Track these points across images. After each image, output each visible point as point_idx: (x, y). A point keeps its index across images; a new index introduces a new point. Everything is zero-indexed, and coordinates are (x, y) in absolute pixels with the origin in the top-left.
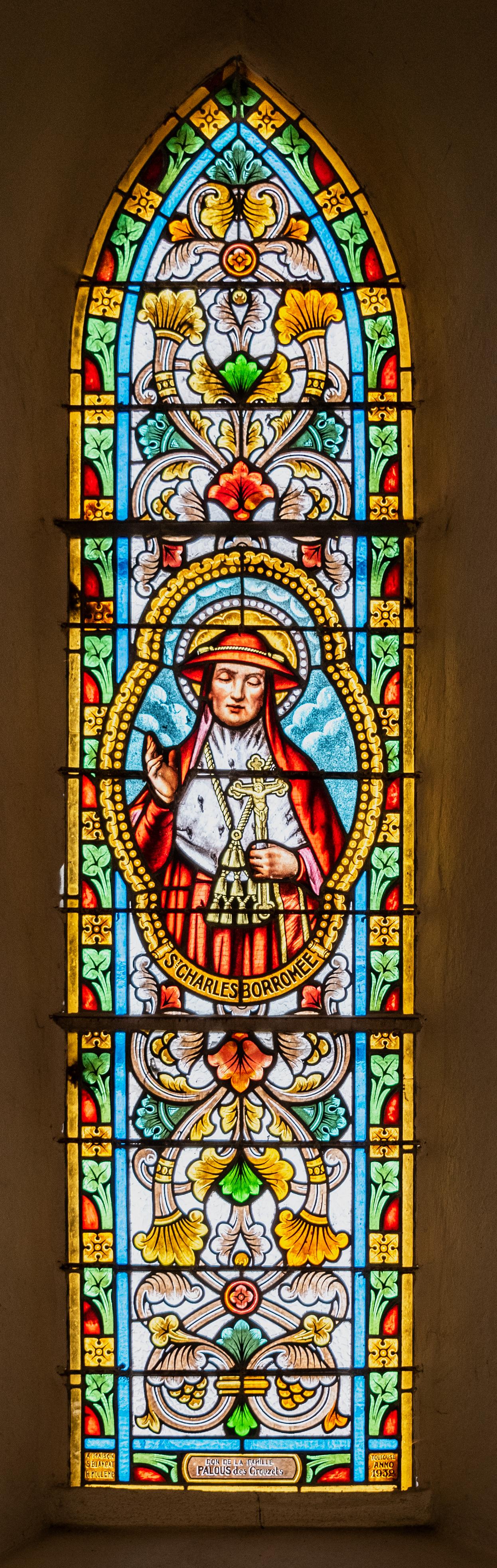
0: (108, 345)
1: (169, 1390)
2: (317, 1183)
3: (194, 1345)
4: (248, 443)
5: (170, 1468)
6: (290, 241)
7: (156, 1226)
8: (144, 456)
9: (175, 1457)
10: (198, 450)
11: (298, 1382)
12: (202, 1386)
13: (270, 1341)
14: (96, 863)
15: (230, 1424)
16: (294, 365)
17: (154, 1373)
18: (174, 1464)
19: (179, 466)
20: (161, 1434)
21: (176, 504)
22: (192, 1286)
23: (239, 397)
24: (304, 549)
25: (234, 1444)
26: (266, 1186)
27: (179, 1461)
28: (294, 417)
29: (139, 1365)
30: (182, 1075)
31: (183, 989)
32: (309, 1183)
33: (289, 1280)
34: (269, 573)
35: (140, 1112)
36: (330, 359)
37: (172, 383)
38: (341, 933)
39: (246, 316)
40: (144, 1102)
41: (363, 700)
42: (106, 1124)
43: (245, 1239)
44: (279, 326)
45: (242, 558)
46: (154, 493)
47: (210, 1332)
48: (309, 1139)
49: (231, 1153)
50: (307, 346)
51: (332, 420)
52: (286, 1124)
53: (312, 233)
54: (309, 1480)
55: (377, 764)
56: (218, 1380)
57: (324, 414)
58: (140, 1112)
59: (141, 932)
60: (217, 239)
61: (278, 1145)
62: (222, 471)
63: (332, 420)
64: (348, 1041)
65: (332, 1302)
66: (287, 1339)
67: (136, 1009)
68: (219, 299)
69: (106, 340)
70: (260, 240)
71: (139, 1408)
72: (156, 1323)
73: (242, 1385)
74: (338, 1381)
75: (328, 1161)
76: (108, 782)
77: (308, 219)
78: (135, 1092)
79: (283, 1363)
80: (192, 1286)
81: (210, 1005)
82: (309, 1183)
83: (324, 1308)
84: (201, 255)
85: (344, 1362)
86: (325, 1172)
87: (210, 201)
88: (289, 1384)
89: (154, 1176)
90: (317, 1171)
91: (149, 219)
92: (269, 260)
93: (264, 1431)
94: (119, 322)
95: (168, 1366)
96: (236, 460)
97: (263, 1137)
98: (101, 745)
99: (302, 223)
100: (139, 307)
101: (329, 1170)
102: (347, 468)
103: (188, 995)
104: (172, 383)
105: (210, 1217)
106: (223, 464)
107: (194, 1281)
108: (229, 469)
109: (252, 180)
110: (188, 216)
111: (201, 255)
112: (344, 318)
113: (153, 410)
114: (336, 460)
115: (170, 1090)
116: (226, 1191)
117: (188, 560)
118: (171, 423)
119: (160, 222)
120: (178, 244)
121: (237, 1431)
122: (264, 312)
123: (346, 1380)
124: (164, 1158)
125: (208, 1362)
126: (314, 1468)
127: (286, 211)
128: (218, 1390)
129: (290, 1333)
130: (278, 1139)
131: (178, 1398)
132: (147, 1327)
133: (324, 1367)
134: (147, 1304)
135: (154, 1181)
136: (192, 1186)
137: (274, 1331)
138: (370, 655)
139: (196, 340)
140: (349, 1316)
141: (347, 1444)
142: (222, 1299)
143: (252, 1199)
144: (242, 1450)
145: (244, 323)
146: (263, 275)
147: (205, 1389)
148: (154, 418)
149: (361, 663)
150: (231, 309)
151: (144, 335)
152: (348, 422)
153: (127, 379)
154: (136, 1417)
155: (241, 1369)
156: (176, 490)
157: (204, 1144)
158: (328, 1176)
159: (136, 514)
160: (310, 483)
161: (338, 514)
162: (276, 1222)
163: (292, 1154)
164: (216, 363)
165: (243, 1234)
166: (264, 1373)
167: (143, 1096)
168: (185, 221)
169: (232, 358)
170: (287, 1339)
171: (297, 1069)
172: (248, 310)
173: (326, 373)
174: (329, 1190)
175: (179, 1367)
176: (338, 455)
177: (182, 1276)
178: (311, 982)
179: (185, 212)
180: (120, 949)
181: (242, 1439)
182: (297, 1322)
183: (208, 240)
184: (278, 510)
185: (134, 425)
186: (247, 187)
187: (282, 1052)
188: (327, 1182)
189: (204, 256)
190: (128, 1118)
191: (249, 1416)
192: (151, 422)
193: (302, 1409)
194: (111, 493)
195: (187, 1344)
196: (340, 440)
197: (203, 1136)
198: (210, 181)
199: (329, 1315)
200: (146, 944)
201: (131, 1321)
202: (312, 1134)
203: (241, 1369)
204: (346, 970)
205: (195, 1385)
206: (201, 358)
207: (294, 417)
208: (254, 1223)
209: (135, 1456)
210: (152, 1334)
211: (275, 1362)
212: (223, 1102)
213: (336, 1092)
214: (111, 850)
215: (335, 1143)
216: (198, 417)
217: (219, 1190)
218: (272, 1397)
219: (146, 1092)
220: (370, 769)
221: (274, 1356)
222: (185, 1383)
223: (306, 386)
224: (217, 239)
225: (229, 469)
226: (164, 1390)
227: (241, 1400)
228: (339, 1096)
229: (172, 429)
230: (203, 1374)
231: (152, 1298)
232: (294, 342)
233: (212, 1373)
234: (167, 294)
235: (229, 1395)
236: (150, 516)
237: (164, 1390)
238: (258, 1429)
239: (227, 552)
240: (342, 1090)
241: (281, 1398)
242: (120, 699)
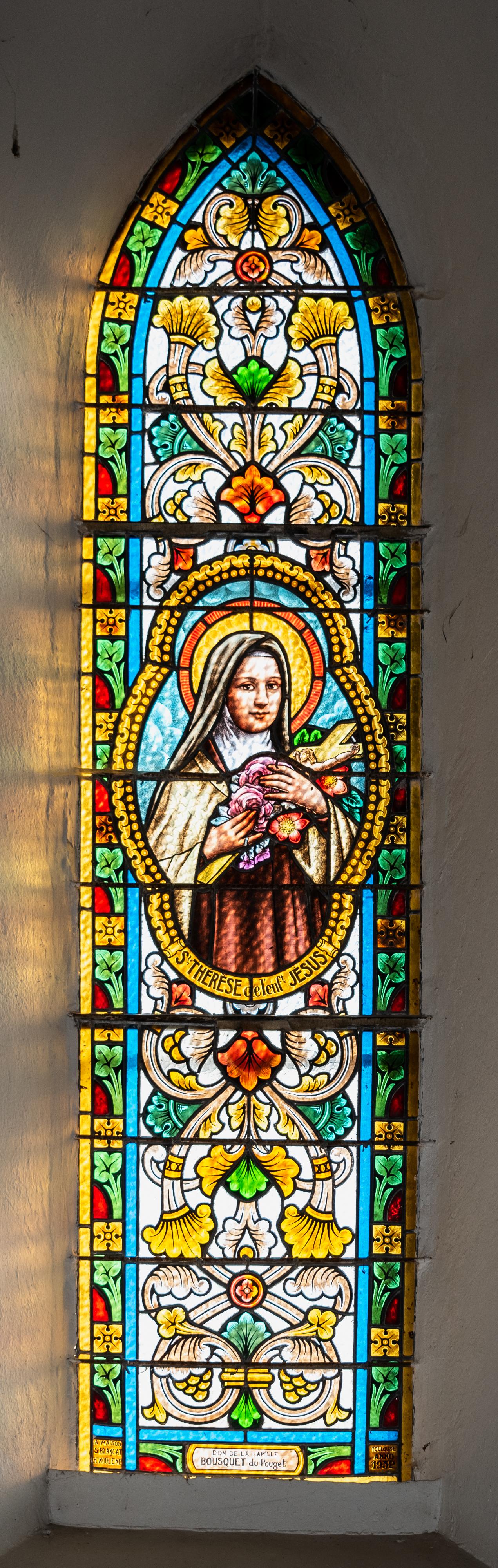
0: (123, 348)
1: (175, 1382)
2: (323, 1180)
3: (201, 1337)
4: (260, 447)
5: (175, 1458)
6: (303, 250)
7: (164, 1221)
8: (157, 457)
9: (180, 1448)
10: (208, 452)
11: (301, 1375)
12: (207, 1377)
13: (273, 1335)
14: (109, 866)
15: (234, 1416)
16: (306, 370)
17: (162, 1364)
18: (179, 1455)
19: (191, 469)
20: (166, 1425)
21: (190, 507)
22: (199, 1279)
23: (252, 401)
24: (313, 553)
25: (238, 1436)
26: (272, 1182)
27: (184, 1452)
28: (305, 421)
29: (145, 1355)
30: (192, 1073)
31: (193, 988)
32: (314, 1180)
33: (293, 1275)
34: (278, 576)
35: (151, 1108)
36: (341, 365)
37: (185, 387)
38: (349, 930)
39: (260, 321)
40: (154, 1099)
41: (370, 703)
42: (117, 1117)
43: (251, 1235)
44: (292, 331)
45: (252, 561)
46: (167, 494)
47: (215, 1325)
48: (315, 1138)
49: (238, 1151)
50: (319, 352)
51: (342, 426)
52: (294, 1123)
53: (325, 244)
54: (310, 1471)
55: (384, 765)
56: (223, 1372)
57: (334, 420)
58: (151, 1108)
59: (153, 931)
60: (232, 248)
61: (285, 1143)
62: (234, 474)
63: (342, 426)
64: (355, 1043)
65: (335, 1297)
66: (292, 1333)
67: (147, 1008)
68: (233, 306)
69: (121, 343)
70: (275, 248)
71: (145, 1399)
72: (163, 1315)
73: (246, 1377)
74: (339, 1374)
75: (333, 1157)
76: (120, 783)
77: (321, 229)
78: (146, 1089)
79: (288, 1356)
80: (199, 1279)
81: (220, 1003)
82: (314, 1180)
83: (328, 1303)
84: (214, 262)
85: (347, 1357)
86: (331, 1169)
87: (226, 211)
88: (291, 1377)
89: (163, 1172)
90: (323, 1168)
91: (165, 226)
92: (280, 267)
93: (268, 1424)
94: (133, 325)
95: (174, 1357)
96: (247, 465)
97: (272, 1135)
98: (113, 747)
99: (315, 232)
100: (154, 311)
101: (334, 1166)
102: (357, 474)
103: (198, 994)
104: (185, 387)
105: (217, 1214)
106: (235, 468)
107: (201, 1274)
108: (241, 472)
109: (267, 189)
110: (203, 225)
111: (214, 262)
112: (356, 326)
113: (164, 411)
114: (346, 466)
115: (181, 1088)
116: (234, 1187)
117: (199, 563)
118: (184, 424)
119: (176, 230)
120: (192, 252)
121: (241, 1422)
122: (278, 318)
123: (348, 1374)
124: (173, 1155)
125: (212, 1354)
126: (315, 1460)
127: (299, 222)
128: (223, 1382)
129: (293, 1327)
130: (284, 1138)
131: (184, 1390)
132: (155, 1319)
133: (327, 1361)
134: (155, 1296)
135: (164, 1177)
136: (200, 1183)
137: (277, 1325)
138: (377, 662)
139: (211, 345)
140: (352, 1310)
141: (348, 1437)
142: (228, 1293)
143: (259, 1194)
144: (245, 1442)
145: (258, 328)
146: (275, 280)
147: (210, 1380)
148: (167, 419)
149: (368, 668)
150: (245, 315)
151: (158, 340)
152: (358, 428)
153: (140, 379)
154: (143, 1408)
155: (247, 1361)
156: (188, 492)
157: (212, 1142)
158: (333, 1173)
159: (149, 514)
160: (319, 488)
161: (348, 519)
162: (282, 1217)
163: (297, 1152)
164: (230, 368)
165: (249, 1230)
166: (269, 1365)
167: (154, 1094)
168: (200, 230)
169: (245, 363)
170: (292, 1333)
171: (304, 1070)
172: (262, 316)
173: (337, 380)
174: (334, 1186)
175: (185, 1359)
176: (348, 460)
177: (189, 1269)
178: (319, 980)
179: (201, 221)
180: (132, 948)
181: (245, 1430)
182: (301, 1317)
183: (223, 249)
184: (287, 516)
185: (147, 426)
186: (262, 197)
187: (290, 1054)
188: (332, 1177)
189: (218, 263)
190: (139, 1115)
191: (251, 1406)
192: (164, 423)
193: (305, 1401)
194: (125, 492)
195: (193, 1336)
196: (349, 446)
197: (212, 1134)
198: (225, 191)
199: (333, 1309)
200: (158, 943)
201: (138, 1312)
202: (317, 1132)
203: (247, 1361)
204: (353, 969)
205: (201, 1377)
206: (215, 364)
207: (305, 421)
208: (260, 1219)
209: (142, 1446)
210: (159, 1325)
211: (280, 1354)
212: (231, 1101)
213: (343, 1092)
214: (124, 850)
215: (339, 1141)
216: (211, 419)
217: (227, 1186)
218: (276, 1390)
219: (156, 1090)
220: (378, 769)
221: (280, 1348)
222: (191, 1375)
223: (316, 392)
224: (232, 248)
225: (241, 472)
226: (170, 1381)
227: (246, 1392)
228: (345, 1096)
229: (184, 431)
230: (209, 1366)
231: (160, 1290)
232: (307, 349)
233: (216, 1365)
234: (180, 299)
235: (233, 1387)
236: (338, 1036)
237: (170, 1381)
238: (261, 1420)
239: (237, 554)
240: (348, 1091)
241: (285, 1391)
242: (132, 702)
